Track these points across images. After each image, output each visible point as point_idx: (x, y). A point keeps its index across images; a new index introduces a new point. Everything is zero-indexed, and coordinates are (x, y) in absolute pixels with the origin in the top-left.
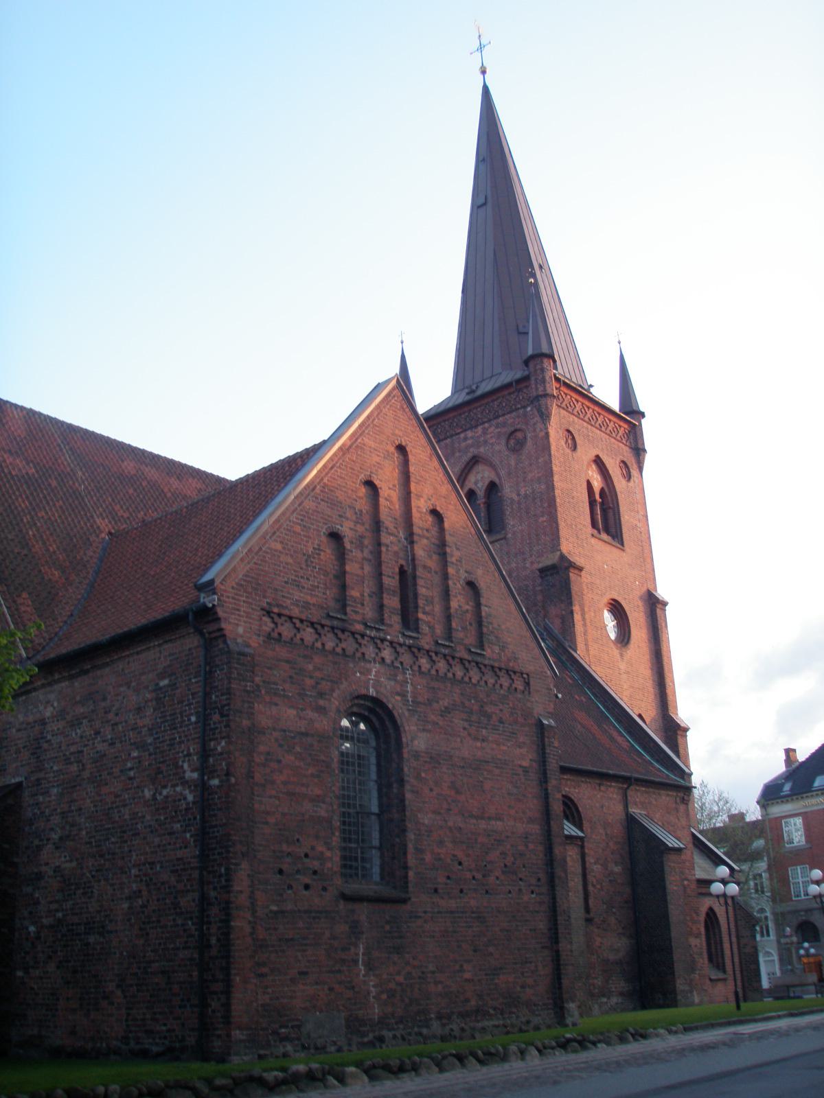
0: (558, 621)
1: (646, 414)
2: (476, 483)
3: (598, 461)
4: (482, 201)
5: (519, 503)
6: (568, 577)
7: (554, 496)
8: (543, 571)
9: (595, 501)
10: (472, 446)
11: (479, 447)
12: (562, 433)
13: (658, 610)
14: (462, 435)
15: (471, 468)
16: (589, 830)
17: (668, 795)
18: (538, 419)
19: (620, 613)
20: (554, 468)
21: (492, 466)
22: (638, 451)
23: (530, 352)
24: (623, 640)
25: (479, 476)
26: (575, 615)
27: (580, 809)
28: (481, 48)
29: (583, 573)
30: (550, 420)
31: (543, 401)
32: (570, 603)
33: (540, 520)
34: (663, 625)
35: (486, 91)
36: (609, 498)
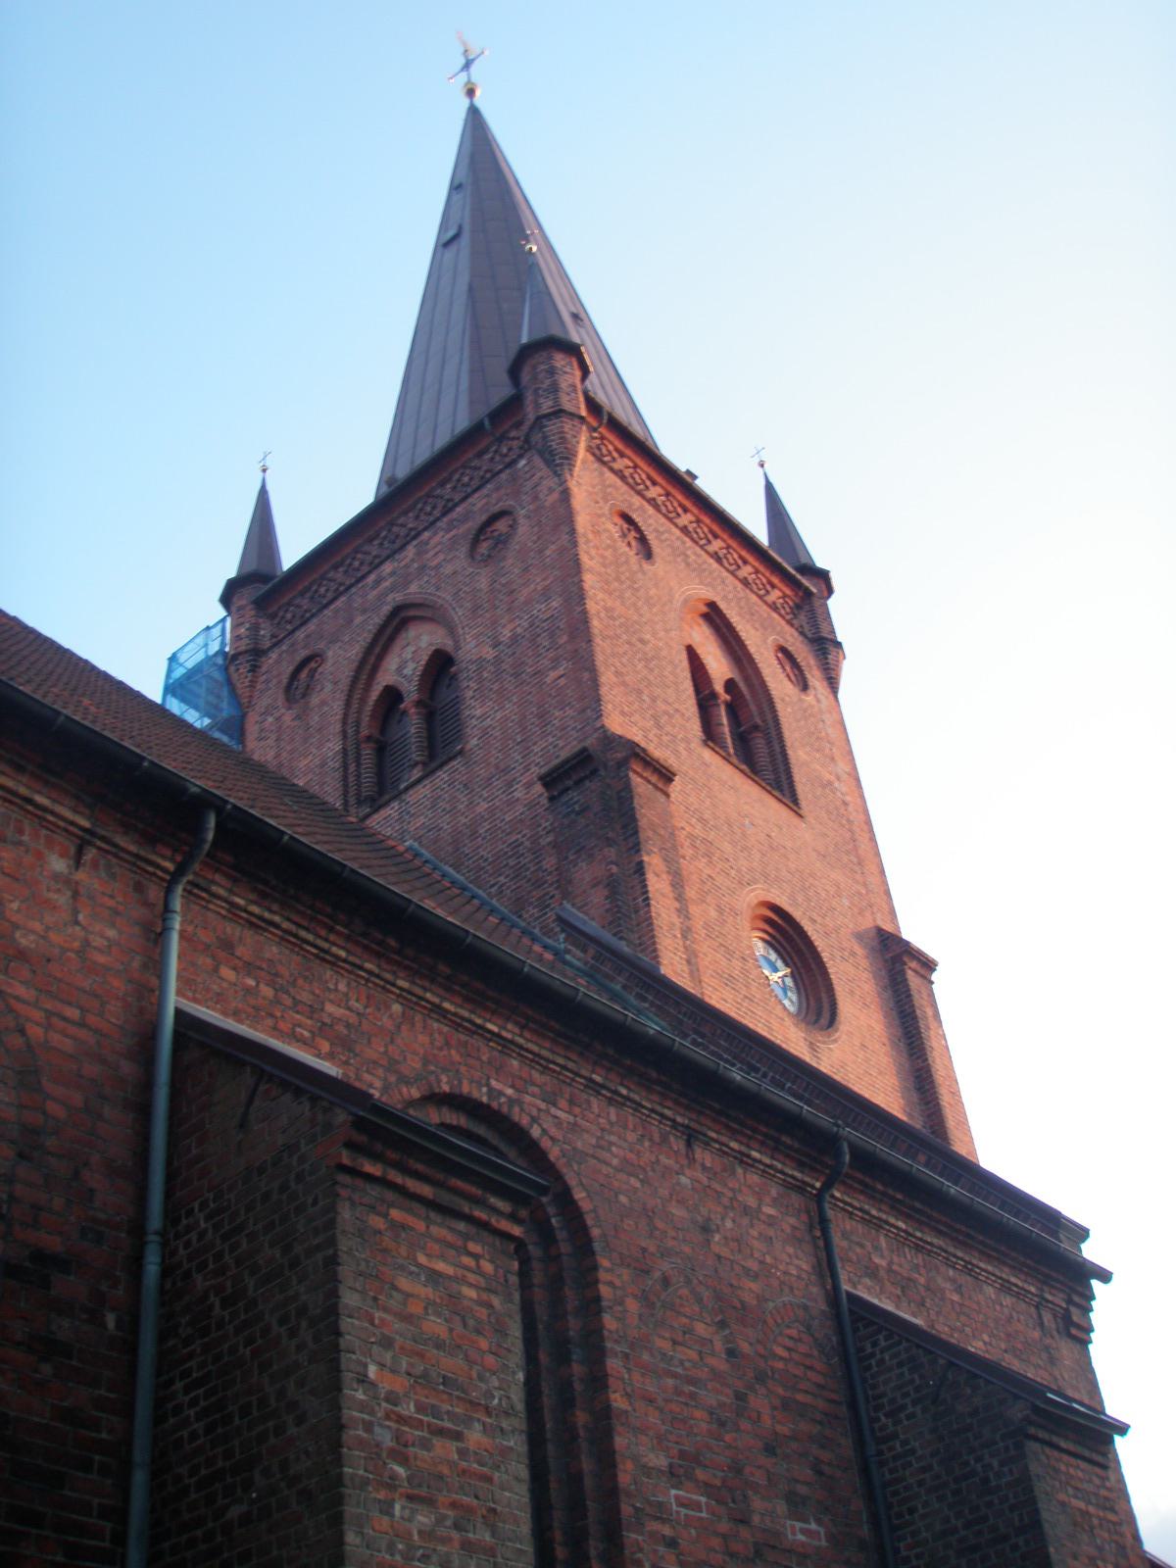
0: (598, 897)
1: (836, 580)
2: (399, 670)
3: (714, 616)
4: (451, 233)
5: (498, 661)
6: (628, 787)
7: (585, 612)
8: (555, 780)
9: (714, 695)
10: (392, 589)
11: (406, 584)
12: (613, 528)
13: (910, 974)
14: (372, 577)
15: (391, 639)
16: (633, 1306)
17: (1006, 1287)
18: (543, 470)
19: (799, 952)
20: (584, 558)
21: (452, 631)
22: (826, 646)
23: (525, 340)
24: (819, 1015)
25: (408, 653)
26: (651, 880)
27: (579, 1195)
28: (467, 65)
29: (675, 788)
30: (572, 466)
31: (552, 427)
32: (637, 848)
33: (548, 680)
34: (929, 1012)
35: (475, 122)
36: (753, 707)
